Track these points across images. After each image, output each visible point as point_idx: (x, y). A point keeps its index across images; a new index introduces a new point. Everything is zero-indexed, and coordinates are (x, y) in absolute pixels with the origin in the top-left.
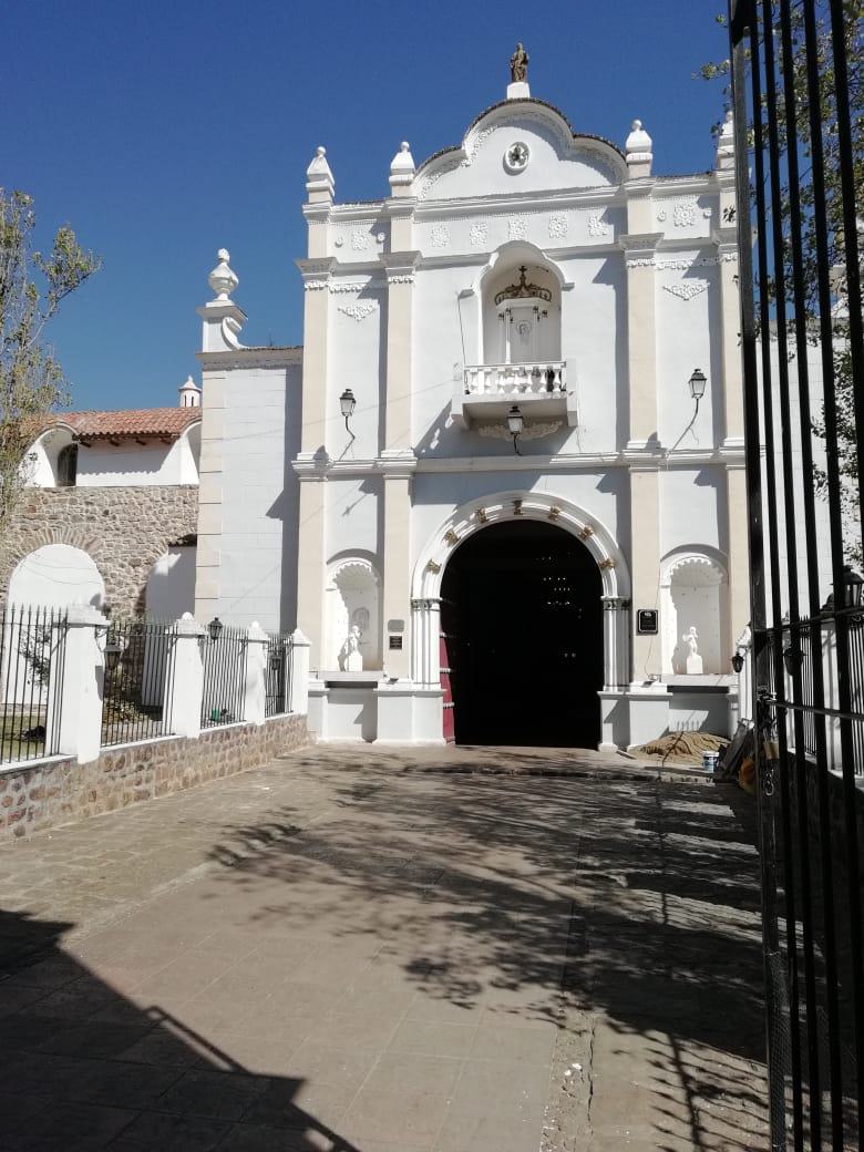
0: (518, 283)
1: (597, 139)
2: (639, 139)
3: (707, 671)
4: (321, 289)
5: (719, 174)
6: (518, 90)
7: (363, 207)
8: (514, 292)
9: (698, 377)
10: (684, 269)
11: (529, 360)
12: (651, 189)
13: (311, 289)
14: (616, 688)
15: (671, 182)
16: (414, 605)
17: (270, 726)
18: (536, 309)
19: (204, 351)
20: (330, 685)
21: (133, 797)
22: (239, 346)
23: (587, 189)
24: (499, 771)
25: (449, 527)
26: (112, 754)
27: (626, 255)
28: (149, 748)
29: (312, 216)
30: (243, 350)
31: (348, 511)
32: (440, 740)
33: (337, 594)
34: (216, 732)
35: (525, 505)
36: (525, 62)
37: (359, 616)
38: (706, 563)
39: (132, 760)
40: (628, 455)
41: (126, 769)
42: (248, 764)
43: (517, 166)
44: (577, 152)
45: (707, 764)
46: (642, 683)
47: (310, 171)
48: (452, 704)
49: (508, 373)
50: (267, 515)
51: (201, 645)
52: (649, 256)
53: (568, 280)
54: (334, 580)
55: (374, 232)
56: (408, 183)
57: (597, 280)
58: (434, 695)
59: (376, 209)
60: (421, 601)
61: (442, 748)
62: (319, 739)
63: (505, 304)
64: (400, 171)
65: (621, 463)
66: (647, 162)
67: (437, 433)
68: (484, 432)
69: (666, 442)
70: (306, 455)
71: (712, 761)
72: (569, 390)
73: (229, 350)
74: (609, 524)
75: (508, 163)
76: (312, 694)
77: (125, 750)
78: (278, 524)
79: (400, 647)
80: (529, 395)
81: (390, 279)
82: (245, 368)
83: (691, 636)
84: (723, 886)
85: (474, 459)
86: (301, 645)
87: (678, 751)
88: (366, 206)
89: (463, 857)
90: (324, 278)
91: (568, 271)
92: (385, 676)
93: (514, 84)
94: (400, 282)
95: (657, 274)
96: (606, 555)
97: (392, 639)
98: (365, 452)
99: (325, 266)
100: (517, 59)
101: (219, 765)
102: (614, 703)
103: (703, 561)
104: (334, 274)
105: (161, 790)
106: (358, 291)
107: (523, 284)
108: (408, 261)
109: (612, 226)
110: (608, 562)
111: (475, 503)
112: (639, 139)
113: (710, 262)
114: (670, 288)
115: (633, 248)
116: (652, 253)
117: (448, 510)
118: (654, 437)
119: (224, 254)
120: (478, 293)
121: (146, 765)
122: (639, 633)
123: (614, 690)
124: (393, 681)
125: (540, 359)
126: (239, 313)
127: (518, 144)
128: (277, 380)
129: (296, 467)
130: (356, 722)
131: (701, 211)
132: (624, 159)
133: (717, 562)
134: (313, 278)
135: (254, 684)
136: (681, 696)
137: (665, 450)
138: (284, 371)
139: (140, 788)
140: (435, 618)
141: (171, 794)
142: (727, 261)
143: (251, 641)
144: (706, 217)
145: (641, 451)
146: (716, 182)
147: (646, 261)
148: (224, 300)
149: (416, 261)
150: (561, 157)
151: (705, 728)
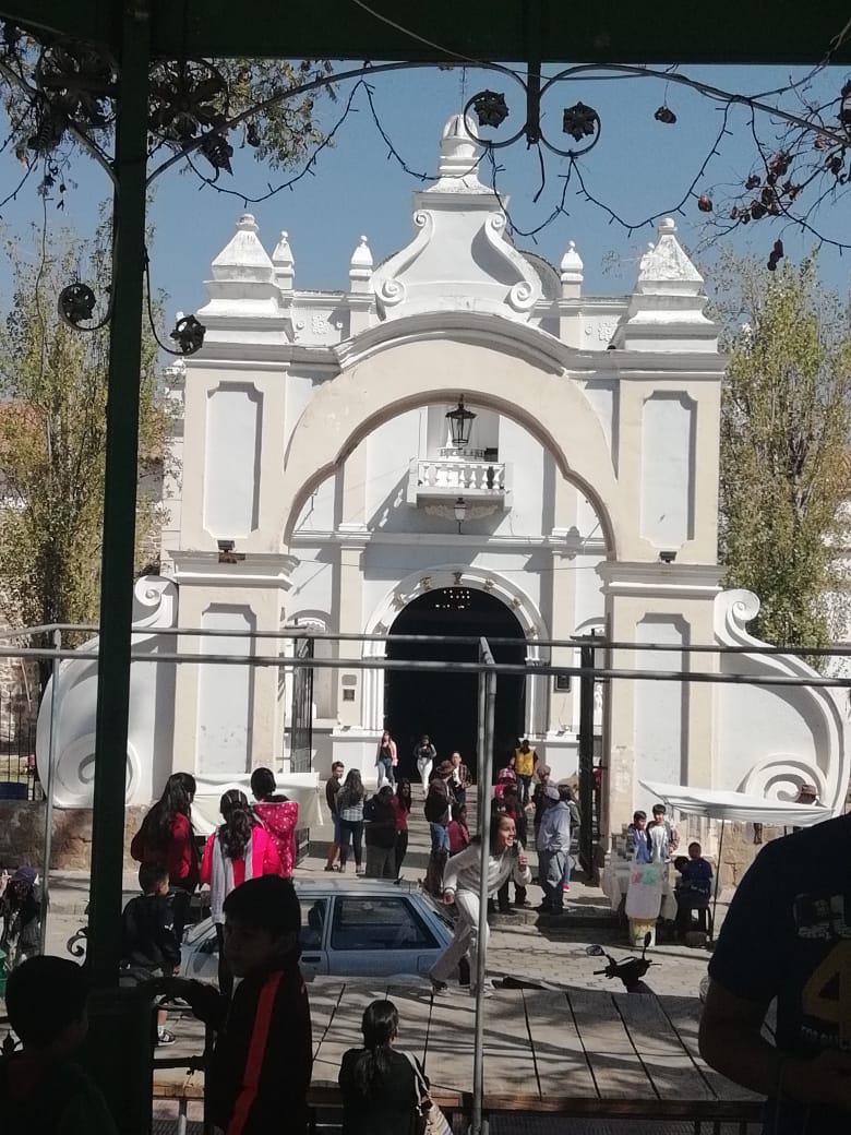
35: (463, 577)
46: (556, 733)
55: (332, 320)
56: (367, 279)
59: (337, 299)
72: (506, 489)
79: (353, 698)
80: (472, 491)
85: (422, 535)
96: (531, 624)
97: (345, 691)
122: (555, 691)
124: (347, 728)
145: (561, 538)
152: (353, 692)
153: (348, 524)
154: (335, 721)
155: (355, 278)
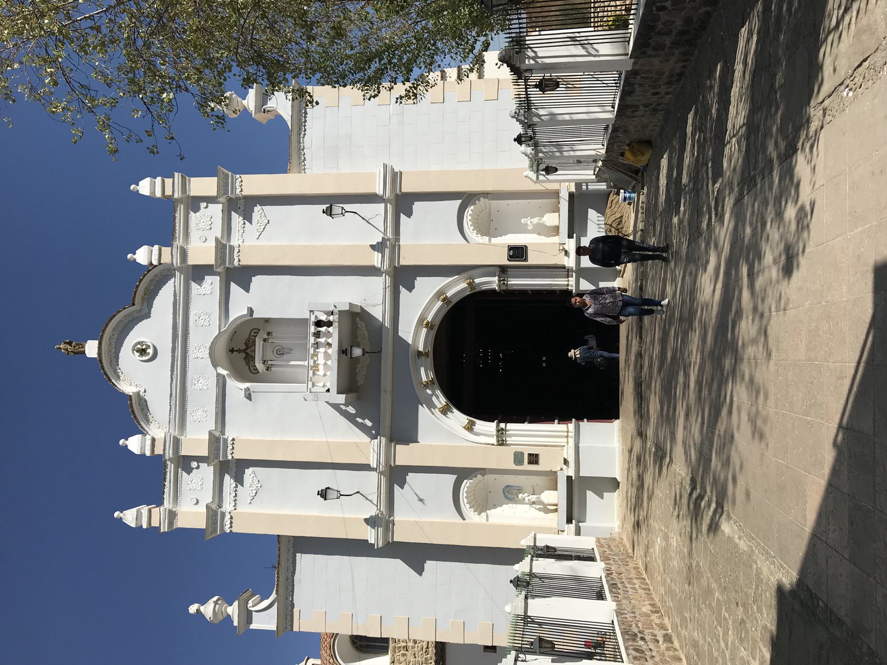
0: (243, 355)
1: (137, 287)
2: (142, 256)
3: (557, 210)
4: (231, 518)
5: (176, 196)
6: (91, 349)
7: (168, 480)
8: (249, 359)
9: (329, 212)
10: (244, 223)
11: (306, 350)
12: (181, 247)
13: (231, 527)
14: (570, 279)
15: (177, 232)
16: (501, 443)
17: (605, 559)
18: (265, 340)
19: (275, 629)
20: (569, 521)
21: (669, 645)
22: (273, 596)
23: (175, 296)
24: (640, 355)
25: (437, 412)
26: (631, 657)
27: (230, 266)
28: (624, 633)
29: (171, 523)
30: (277, 591)
31: (421, 500)
32: (617, 423)
33: (492, 512)
34: (611, 591)
35: (421, 349)
36: (70, 344)
37: (510, 495)
38: (471, 210)
39: (636, 644)
40: (386, 266)
41: (644, 647)
42: (639, 573)
43: (150, 351)
44: (146, 304)
45: (630, 198)
46: (566, 258)
47: (133, 525)
48: (585, 420)
49: (315, 367)
50: (420, 574)
51: (534, 597)
52: (232, 248)
53: (245, 312)
54: (479, 514)
55: (189, 471)
56: (153, 440)
57: (247, 290)
58: (577, 430)
59: (171, 468)
60: (498, 437)
61: (622, 422)
62: (617, 530)
63: (259, 365)
64: (143, 447)
65: (392, 274)
66: (160, 250)
67: (359, 420)
68: (361, 380)
69: (378, 238)
70: (371, 535)
71: (628, 195)
72: (332, 308)
73: (276, 605)
74: (439, 283)
75: (147, 358)
76: (578, 532)
77: (627, 648)
78: (429, 565)
79: (537, 455)
80: (334, 340)
81: (230, 457)
82: (293, 591)
83: (529, 222)
84: (718, 110)
85: (382, 389)
86: (535, 539)
87: (619, 226)
88: (168, 477)
89: (707, 321)
90: (223, 515)
91: (238, 311)
92: (561, 470)
93: (86, 352)
94: (233, 448)
95: (247, 243)
96: (464, 285)
97: (530, 463)
98: (371, 482)
99: (214, 515)
100: (67, 350)
101: (641, 592)
102: (582, 281)
103: (470, 212)
104: (220, 507)
105: (662, 627)
106: (236, 486)
107: (244, 351)
108: (216, 442)
109: (206, 277)
110: (469, 284)
111: (418, 390)
112: (142, 256)
113: (241, 204)
114: (258, 234)
115: (224, 260)
116: (230, 246)
117: (423, 411)
118: (373, 247)
119: (193, 609)
120: (248, 385)
121: (640, 635)
122: (526, 260)
123: (572, 281)
124: (566, 462)
125: (306, 338)
126: (245, 595)
127: (133, 350)
128: (305, 562)
129: (380, 545)
130: (602, 497)
131: (202, 210)
132: (156, 266)
133: (472, 202)
134: (222, 526)
135: (572, 569)
136: (576, 228)
137: (383, 238)
138: (298, 555)
139: (661, 640)
140: (512, 427)
141: (666, 620)
142: (241, 191)
143: (531, 570)
144: (207, 207)
145: (383, 257)
146: (182, 199)
147: (236, 251)
148: (233, 610)
149: (217, 434)
150: (148, 316)
151: (601, 211)
152: (530, 455)
153: (371, 459)
154: (559, 473)
155: (153, 450)
